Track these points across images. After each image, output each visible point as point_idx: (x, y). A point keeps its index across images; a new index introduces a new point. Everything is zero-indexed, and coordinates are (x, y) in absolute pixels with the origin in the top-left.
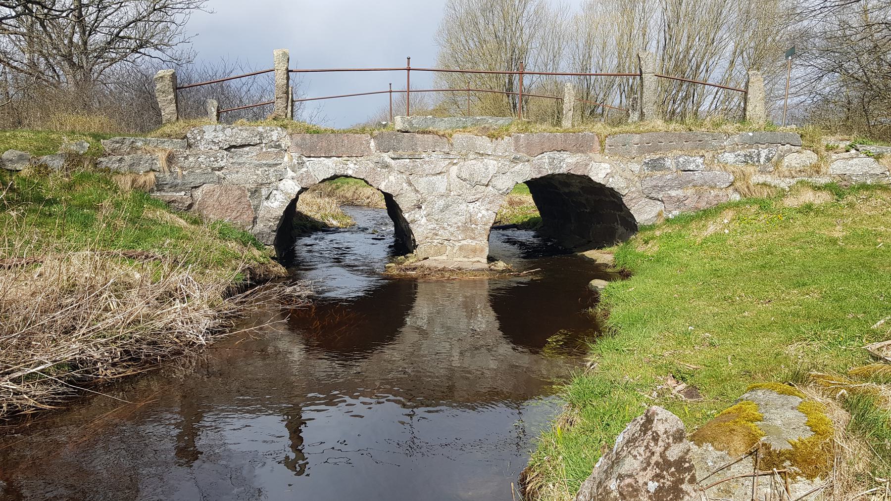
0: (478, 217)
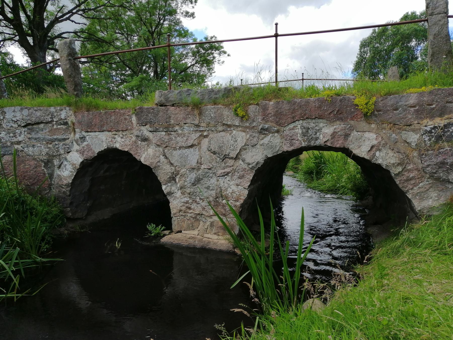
0: (228, 192)
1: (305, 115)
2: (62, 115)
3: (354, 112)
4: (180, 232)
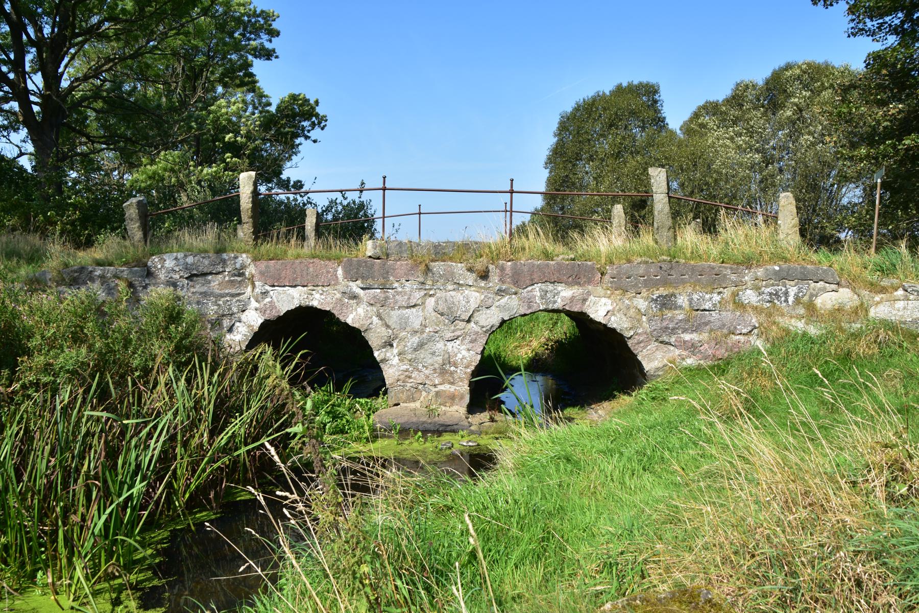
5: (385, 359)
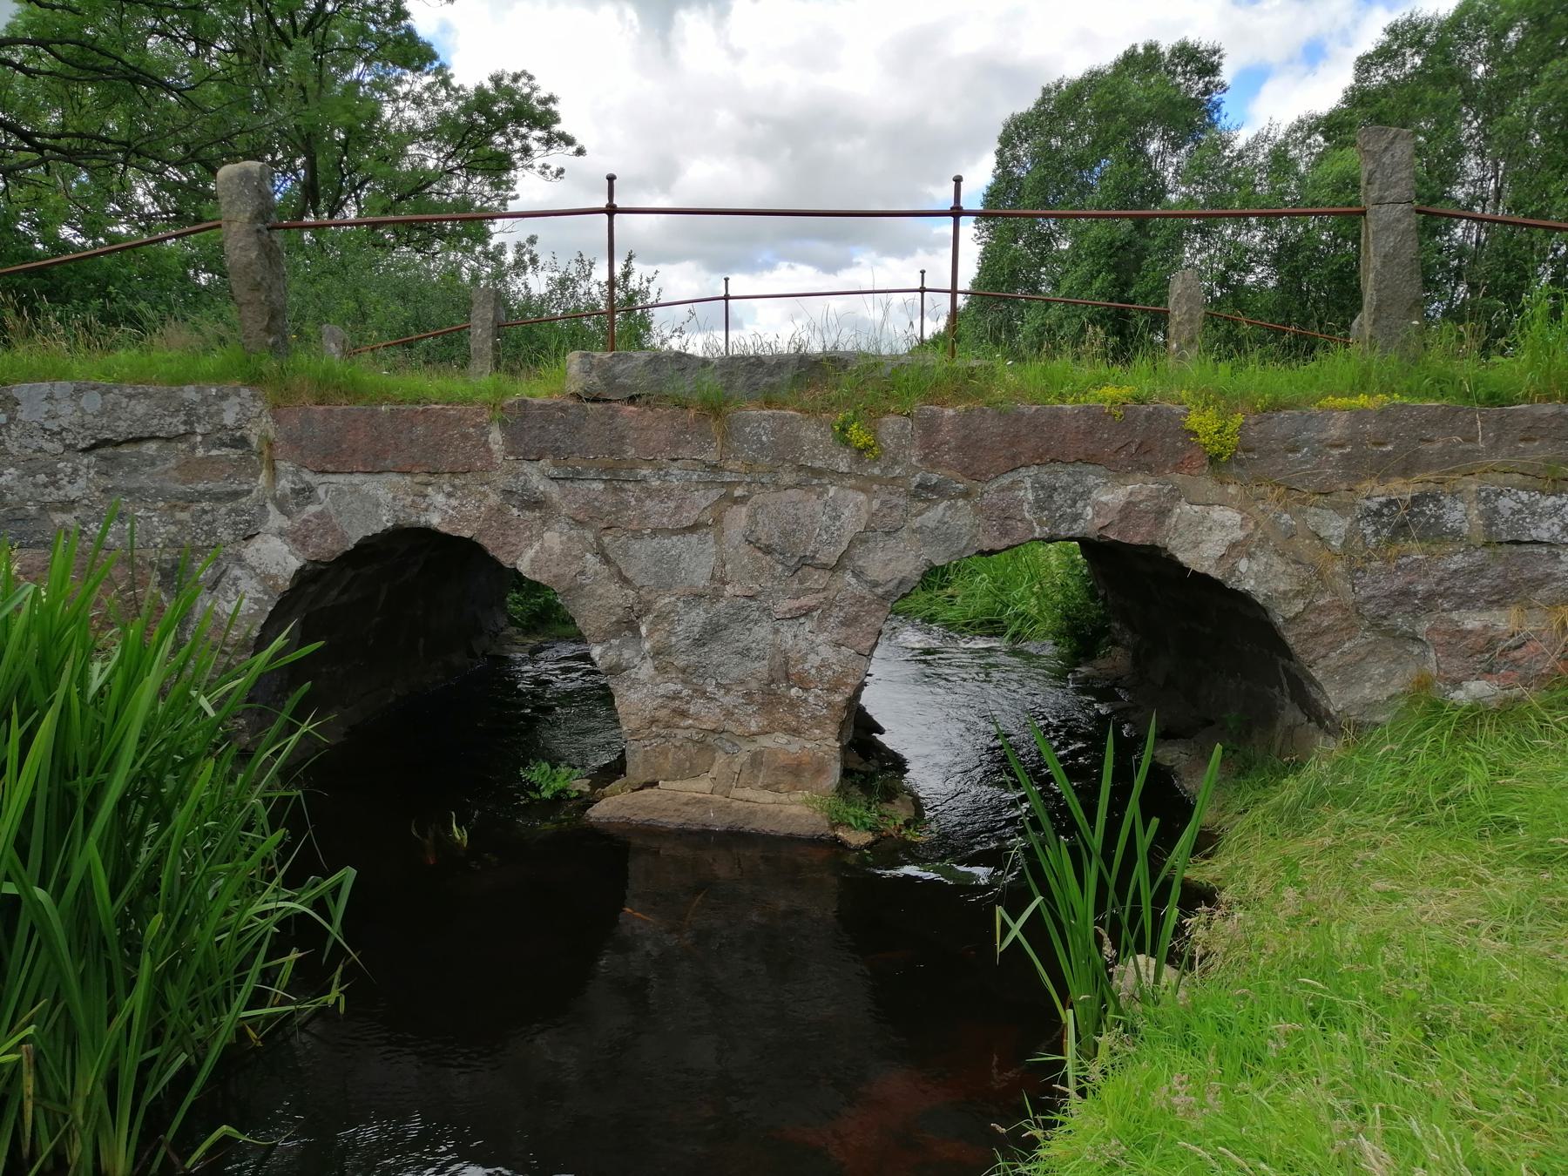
0: (807, 666)
1: (1047, 451)
2: (224, 415)
3: (1182, 451)
4: (654, 784)
5: (618, 665)
